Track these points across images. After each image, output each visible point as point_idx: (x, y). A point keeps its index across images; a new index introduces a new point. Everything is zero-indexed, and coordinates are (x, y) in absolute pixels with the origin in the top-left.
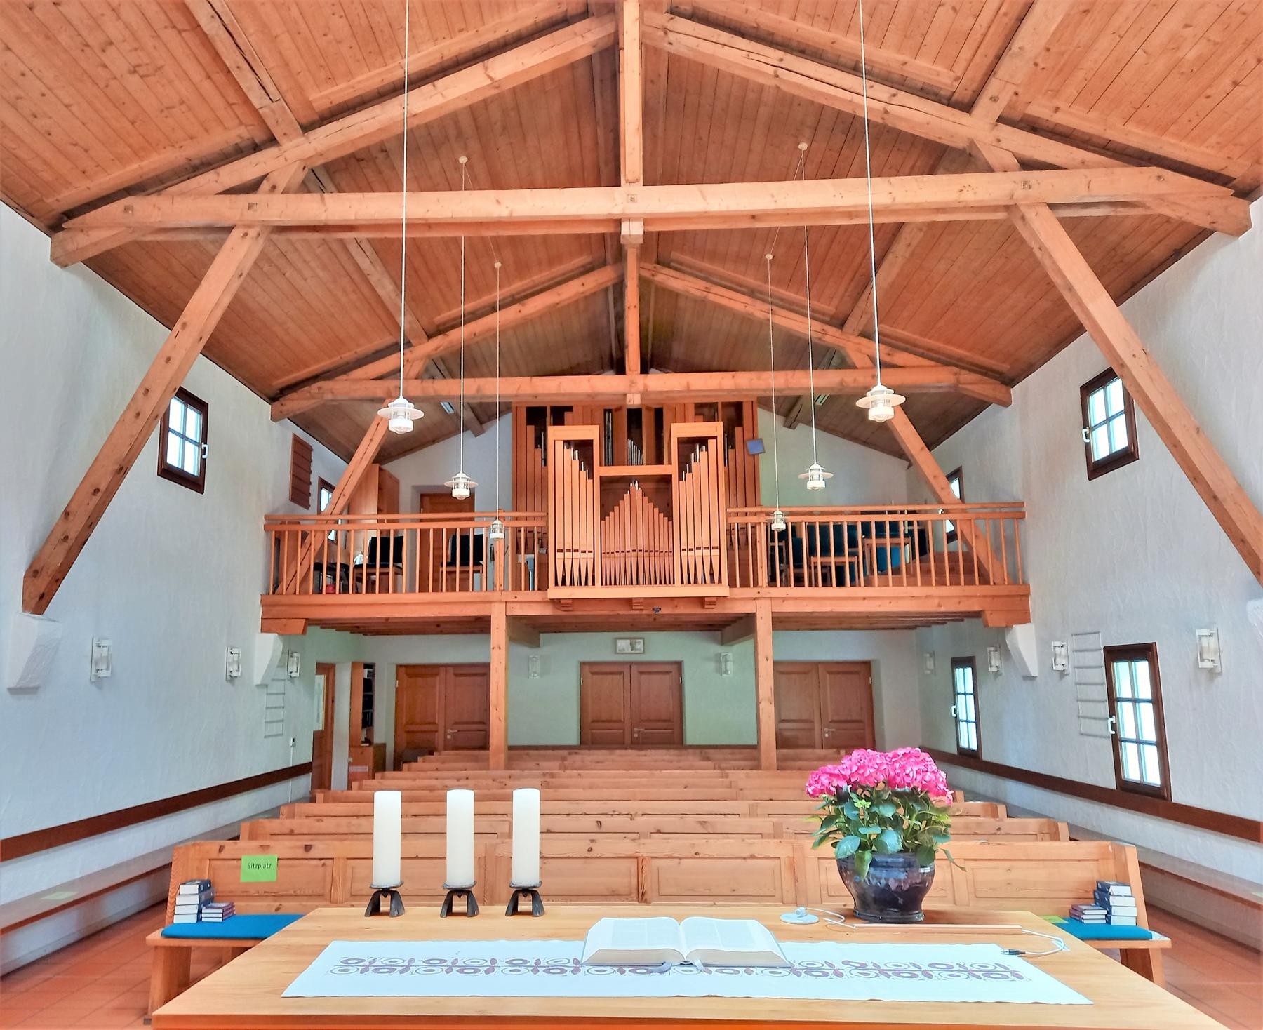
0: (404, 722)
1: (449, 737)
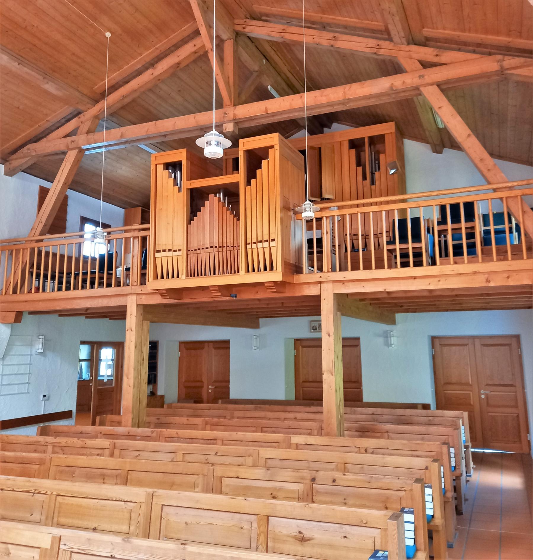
0: (184, 381)
1: (210, 391)
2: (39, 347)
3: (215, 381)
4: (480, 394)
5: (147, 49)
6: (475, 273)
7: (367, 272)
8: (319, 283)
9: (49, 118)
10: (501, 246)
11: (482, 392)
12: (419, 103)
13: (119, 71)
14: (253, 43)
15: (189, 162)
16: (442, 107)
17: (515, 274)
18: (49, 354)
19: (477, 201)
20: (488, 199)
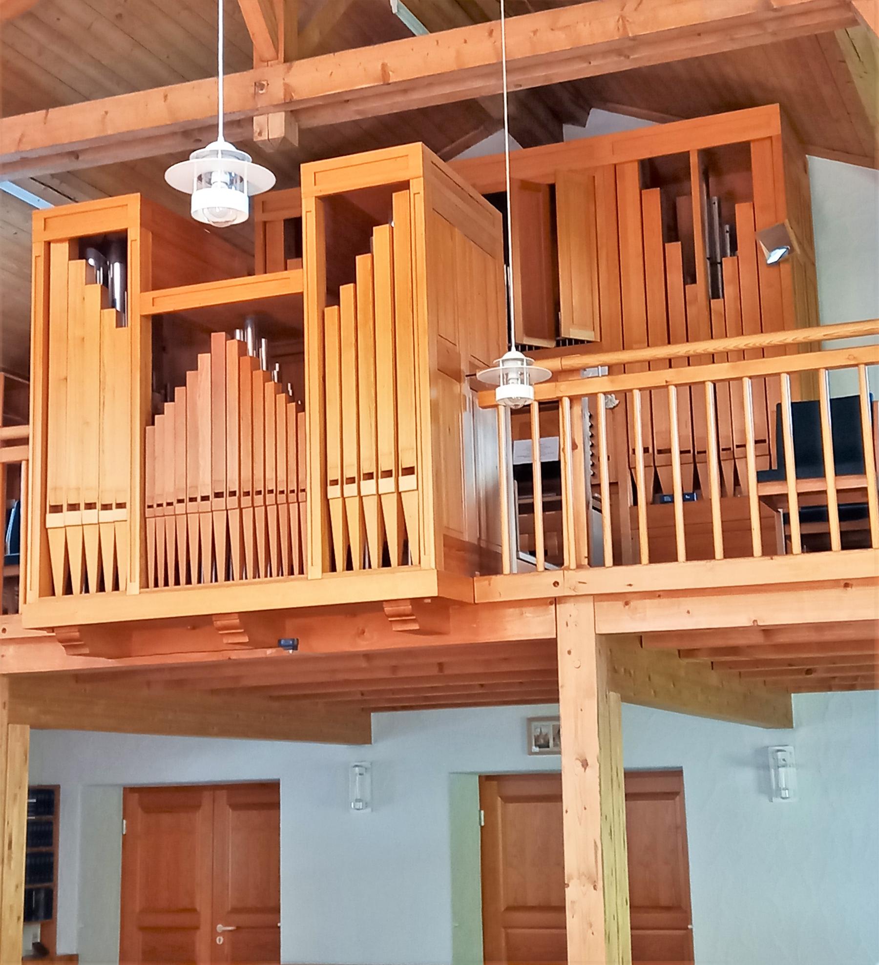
0: (137, 910)
1: (220, 940)
3: (235, 911)
7: (780, 561)
8: (551, 604)
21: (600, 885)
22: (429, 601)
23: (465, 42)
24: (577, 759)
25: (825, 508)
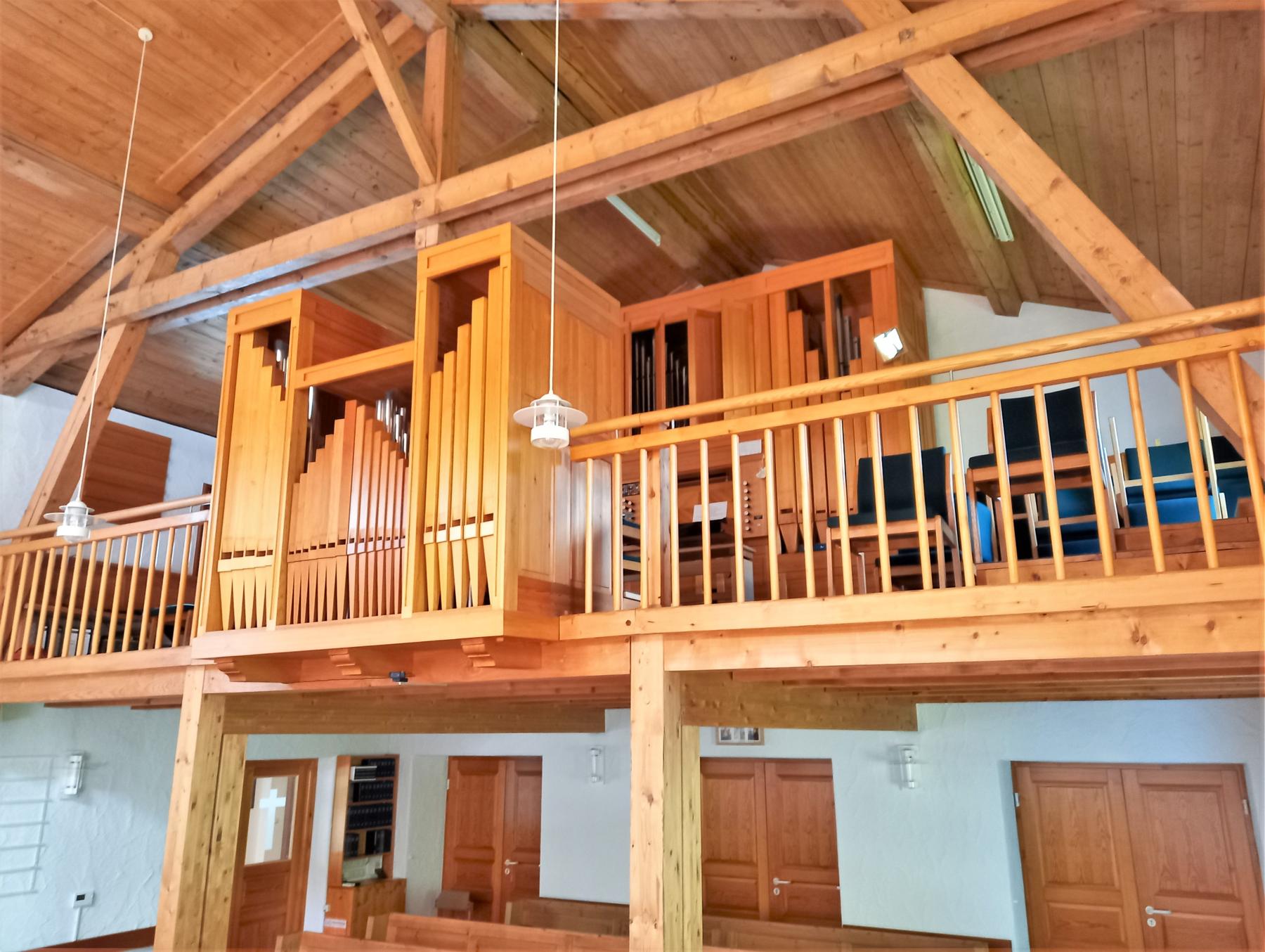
1: (507, 871)
2: (69, 781)
3: (518, 850)
4: (1143, 917)
5: (262, 75)
6: (1092, 611)
7: (832, 602)
8: (627, 641)
9: (71, 259)
10: (1177, 526)
11: (1150, 910)
12: (938, 167)
13: (206, 134)
14: (519, 51)
15: (312, 325)
16: (969, 112)
17: (1234, 615)
18: (101, 798)
19: (1089, 377)
20: (1124, 371)
21: (660, 923)
22: (502, 640)
23: (571, 147)
24: (643, 794)
25: (915, 554)
